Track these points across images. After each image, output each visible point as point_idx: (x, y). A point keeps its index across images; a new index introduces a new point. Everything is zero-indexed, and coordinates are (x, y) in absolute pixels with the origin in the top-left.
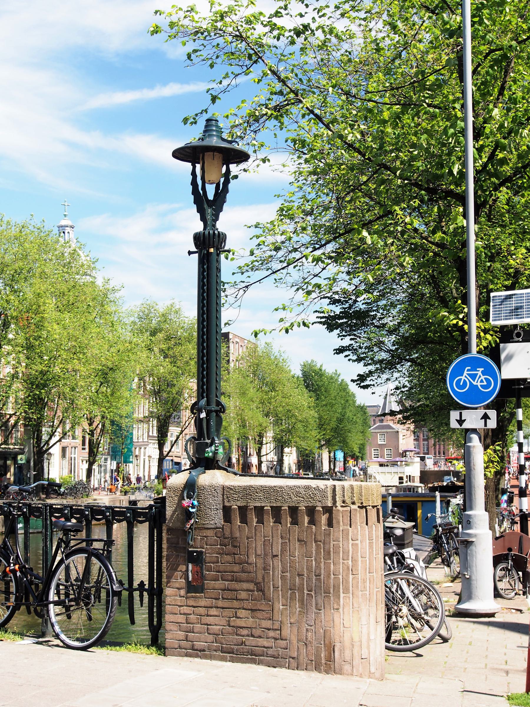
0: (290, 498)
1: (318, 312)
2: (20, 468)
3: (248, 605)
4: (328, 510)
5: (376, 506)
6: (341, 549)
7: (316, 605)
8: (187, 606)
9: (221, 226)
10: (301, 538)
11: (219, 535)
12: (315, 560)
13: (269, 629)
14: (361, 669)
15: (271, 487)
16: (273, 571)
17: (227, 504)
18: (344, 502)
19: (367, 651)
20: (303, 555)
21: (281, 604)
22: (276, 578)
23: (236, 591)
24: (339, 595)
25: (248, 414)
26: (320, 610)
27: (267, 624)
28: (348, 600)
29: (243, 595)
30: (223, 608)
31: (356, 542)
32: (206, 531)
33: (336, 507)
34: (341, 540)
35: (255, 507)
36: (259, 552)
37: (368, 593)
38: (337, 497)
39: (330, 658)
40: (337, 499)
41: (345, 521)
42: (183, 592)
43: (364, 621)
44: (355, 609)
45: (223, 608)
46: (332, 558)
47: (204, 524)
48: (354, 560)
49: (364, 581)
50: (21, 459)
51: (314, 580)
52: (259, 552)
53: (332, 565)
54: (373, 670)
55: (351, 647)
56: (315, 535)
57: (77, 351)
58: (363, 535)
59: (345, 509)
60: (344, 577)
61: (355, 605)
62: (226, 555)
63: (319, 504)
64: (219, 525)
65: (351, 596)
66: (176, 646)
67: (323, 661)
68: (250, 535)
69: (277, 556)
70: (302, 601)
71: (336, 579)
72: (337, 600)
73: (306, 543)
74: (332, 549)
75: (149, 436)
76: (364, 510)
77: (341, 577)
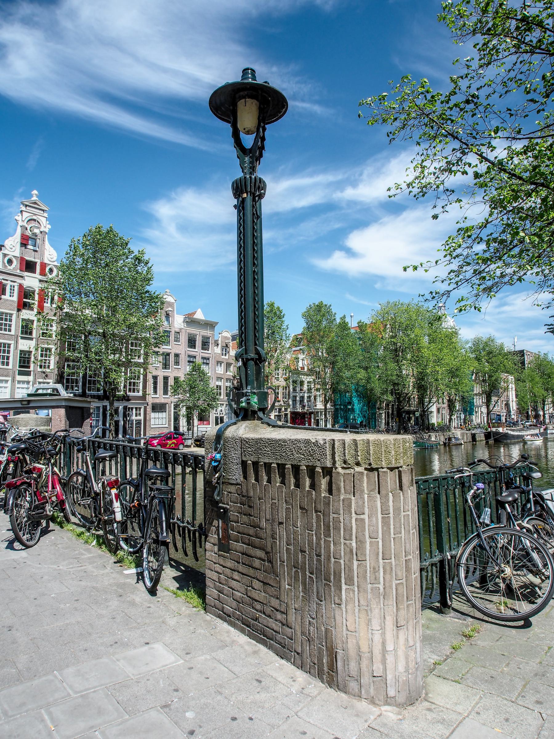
0: (292, 454)
1: (548, 325)
2: (417, 418)
3: (261, 575)
4: (328, 472)
5: (398, 468)
6: (342, 524)
7: (318, 593)
8: (219, 564)
9: (260, 173)
10: (303, 506)
11: (239, 493)
12: (316, 534)
13: (277, 610)
14: (372, 691)
15: (277, 441)
16: (279, 541)
17: (244, 459)
18: (345, 462)
19: (381, 667)
20: (304, 527)
21: (286, 583)
22: (282, 550)
23: (252, 557)
24: (341, 586)
25: (536, 390)
26: (321, 601)
27: (275, 602)
28: (352, 595)
29: (257, 563)
30: (243, 574)
31: (362, 516)
32: (230, 486)
33: (336, 468)
34: (342, 512)
35: (265, 463)
36: (268, 517)
37: (381, 587)
38: (336, 455)
39: (332, 667)
40: (337, 459)
41: (347, 488)
42: (216, 548)
43: (376, 624)
44: (362, 608)
45: (243, 574)
46: (332, 535)
47: (229, 479)
48: (360, 542)
49: (375, 570)
50: (417, 414)
51: (315, 560)
52: (268, 517)
53: (332, 545)
54: (392, 692)
55: (358, 658)
56: (315, 503)
57: (438, 361)
58: (373, 509)
59: (347, 471)
60: (347, 562)
61: (362, 602)
62: (245, 515)
63: (318, 464)
64: (239, 481)
65: (356, 589)
66: (213, 604)
67: (326, 669)
68: (261, 496)
69: (282, 523)
70: (304, 584)
71: (337, 563)
72: (338, 591)
73: (307, 511)
74: (331, 524)
75: (482, 402)
76: (376, 473)
77: (342, 561)
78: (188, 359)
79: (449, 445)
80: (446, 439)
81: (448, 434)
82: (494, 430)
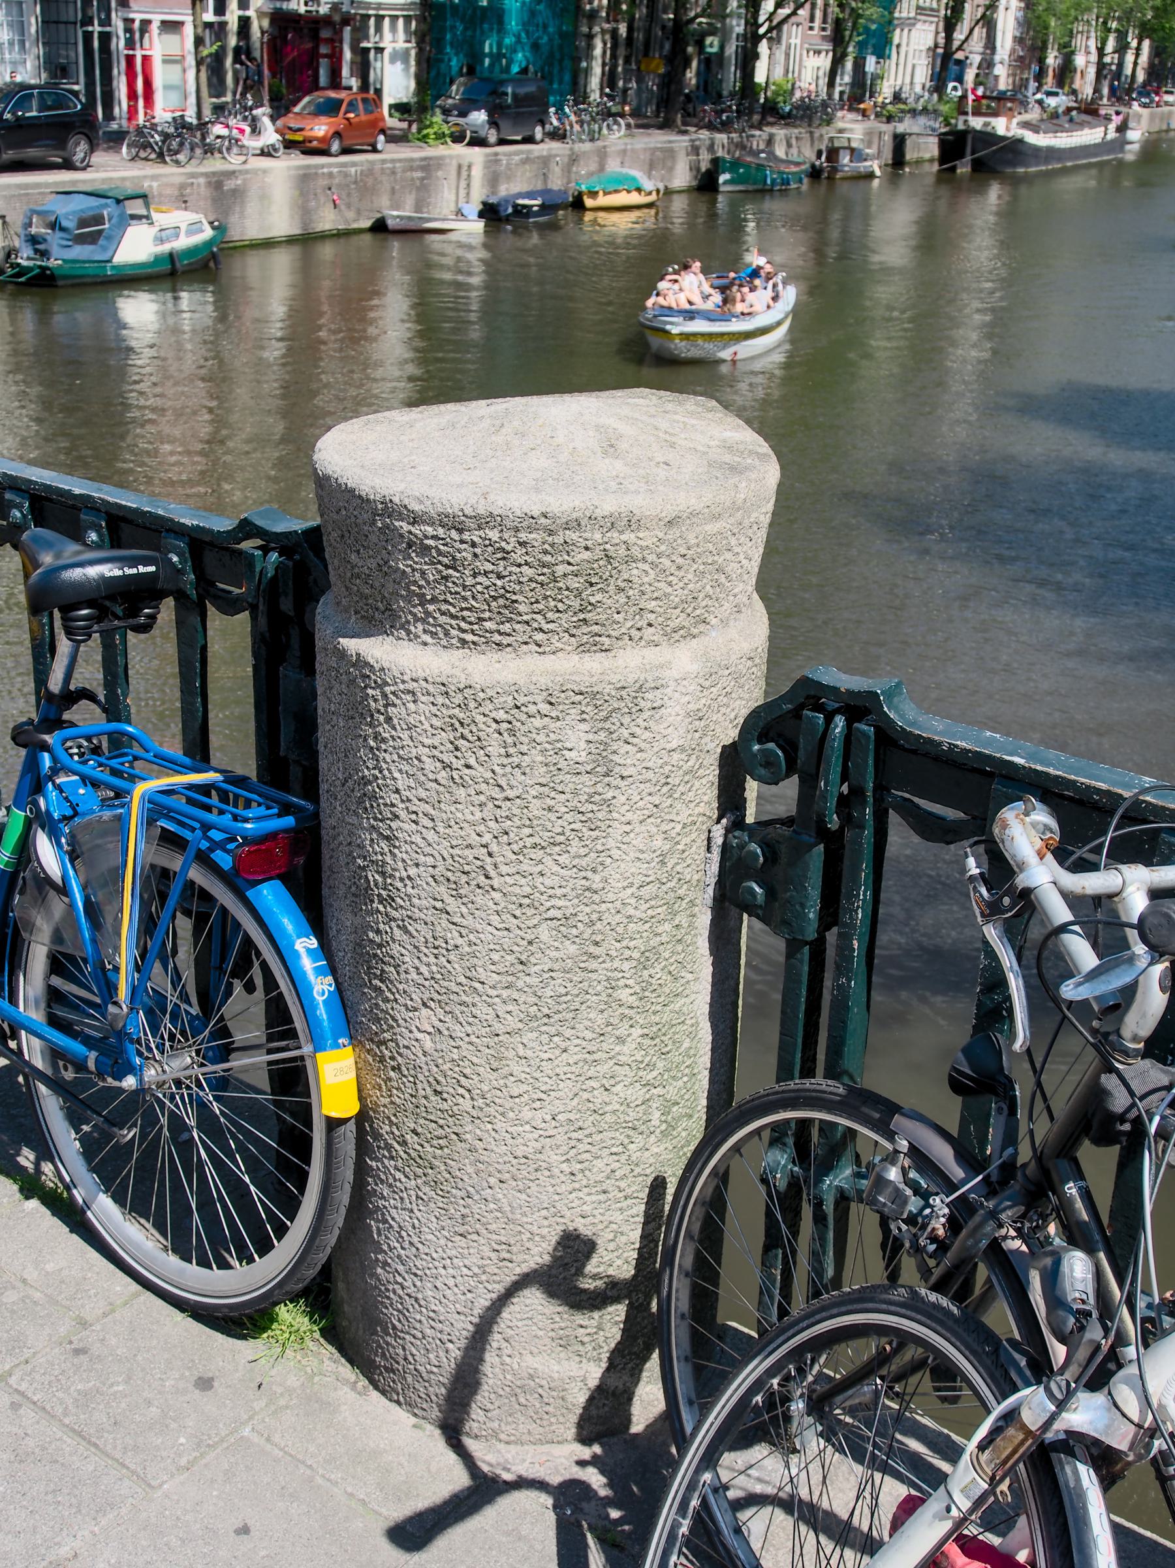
78: (465, 163)
79: (831, 178)
80: (819, 154)
81: (828, 132)
82: (977, 123)
